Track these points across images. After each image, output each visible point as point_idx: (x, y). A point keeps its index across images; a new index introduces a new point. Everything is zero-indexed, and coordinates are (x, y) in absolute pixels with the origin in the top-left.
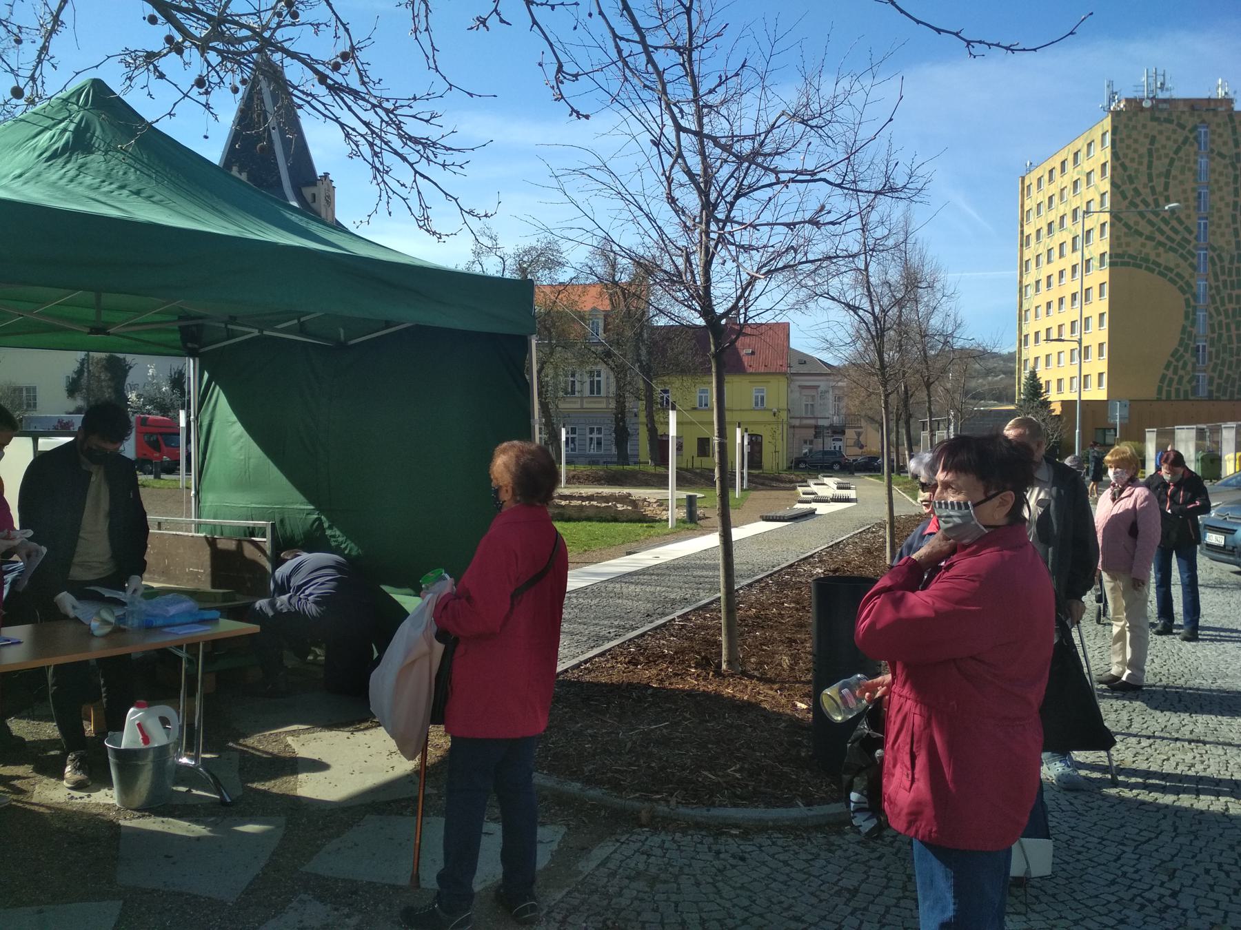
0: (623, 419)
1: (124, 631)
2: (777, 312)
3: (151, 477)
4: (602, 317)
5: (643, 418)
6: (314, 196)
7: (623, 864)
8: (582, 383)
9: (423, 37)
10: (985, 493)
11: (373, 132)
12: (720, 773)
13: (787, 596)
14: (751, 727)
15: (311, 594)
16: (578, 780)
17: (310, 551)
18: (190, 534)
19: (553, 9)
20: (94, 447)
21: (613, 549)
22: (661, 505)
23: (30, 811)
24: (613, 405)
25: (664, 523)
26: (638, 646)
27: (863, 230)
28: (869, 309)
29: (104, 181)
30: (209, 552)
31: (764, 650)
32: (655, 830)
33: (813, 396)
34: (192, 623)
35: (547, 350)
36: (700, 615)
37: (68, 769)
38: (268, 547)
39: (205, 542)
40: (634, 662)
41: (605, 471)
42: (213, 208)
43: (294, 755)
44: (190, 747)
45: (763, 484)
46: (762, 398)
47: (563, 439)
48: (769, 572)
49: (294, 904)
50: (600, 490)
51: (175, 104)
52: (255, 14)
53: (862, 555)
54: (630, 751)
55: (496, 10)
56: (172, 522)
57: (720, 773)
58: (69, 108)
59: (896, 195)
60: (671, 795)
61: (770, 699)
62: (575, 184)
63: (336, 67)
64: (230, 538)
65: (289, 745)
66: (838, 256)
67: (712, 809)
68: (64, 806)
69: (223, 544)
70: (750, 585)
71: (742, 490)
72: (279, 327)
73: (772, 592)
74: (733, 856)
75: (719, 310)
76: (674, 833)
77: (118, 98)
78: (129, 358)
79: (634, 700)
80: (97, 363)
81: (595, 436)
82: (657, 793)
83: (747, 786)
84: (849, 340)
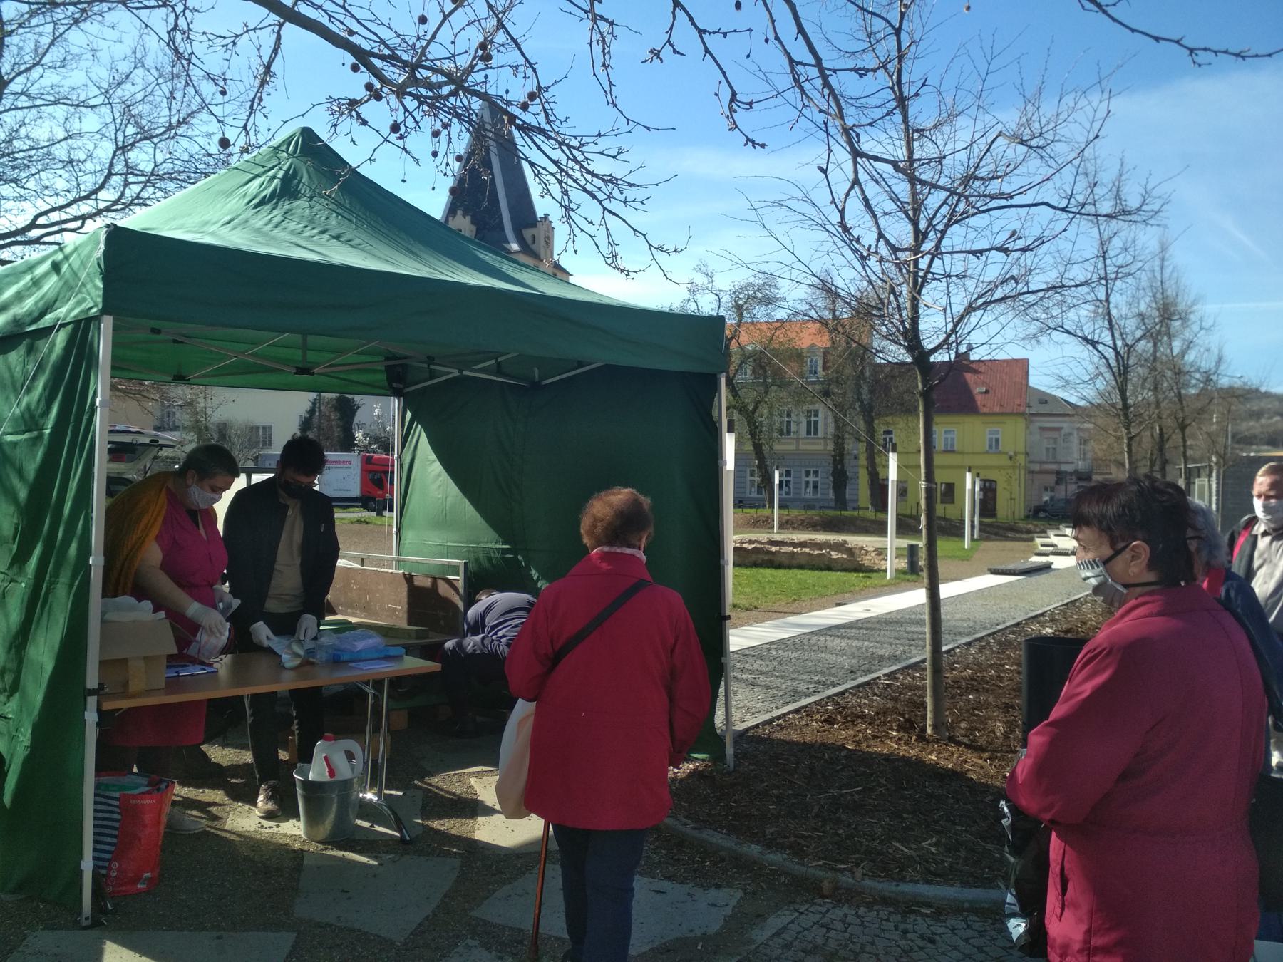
0: (842, 460)
1: (313, 664)
2: (993, 347)
3: (374, 514)
4: (822, 354)
5: (863, 460)
6: (534, 237)
7: (800, 936)
8: (798, 424)
9: (600, 71)
10: (1113, 545)
11: (562, 170)
12: (913, 846)
13: (1009, 657)
14: (953, 797)
15: (504, 636)
16: (758, 842)
17: (501, 591)
18: (390, 571)
19: (725, 37)
20: (290, 480)
21: (824, 600)
22: (880, 554)
23: (222, 838)
24: (831, 446)
25: (882, 574)
26: (837, 704)
27: (1104, 257)
28: (1111, 343)
29: (306, 227)
30: (406, 589)
31: (976, 715)
32: (838, 903)
33: (1055, 440)
34: (379, 659)
35: (762, 389)
36: (909, 674)
37: (261, 798)
38: (461, 585)
39: (403, 579)
40: (830, 721)
41: (821, 517)
42: (409, 250)
43: (474, 797)
44: (374, 783)
45: (996, 534)
46: (997, 440)
47: (777, 481)
48: (993, 630)
49: (460, 949)
50: (813, 537)
51: (375, 150)
52: (449, 58)
53: (1101, 615)
54: (817, 816)
55: (669, 41)
56: (374, 559)
57: (913, 846)
58: (279, 155)
59: (1130, 218)
60: (857, 865)
61: (977, 769)
62: (773, 216)
63: (524, 107)
64: (426, 576)
65: (470, 787)
66: (1063, 286)
67: (901, 884)
68: (253, 835)
69: (419, 582)
70: (969, 644)
71: (972, 539)
72: (476, 367)
73: (993, 652)
74: (922, 937)
75: (928, 345)
76: (858, 907)
77: (326, 145)
78: (357, 398)
79: (826, 761)
80: (328, 403)
81: (811, 479)
82: (843, 862)
83: (943, 862)
84: (1087, 378)
